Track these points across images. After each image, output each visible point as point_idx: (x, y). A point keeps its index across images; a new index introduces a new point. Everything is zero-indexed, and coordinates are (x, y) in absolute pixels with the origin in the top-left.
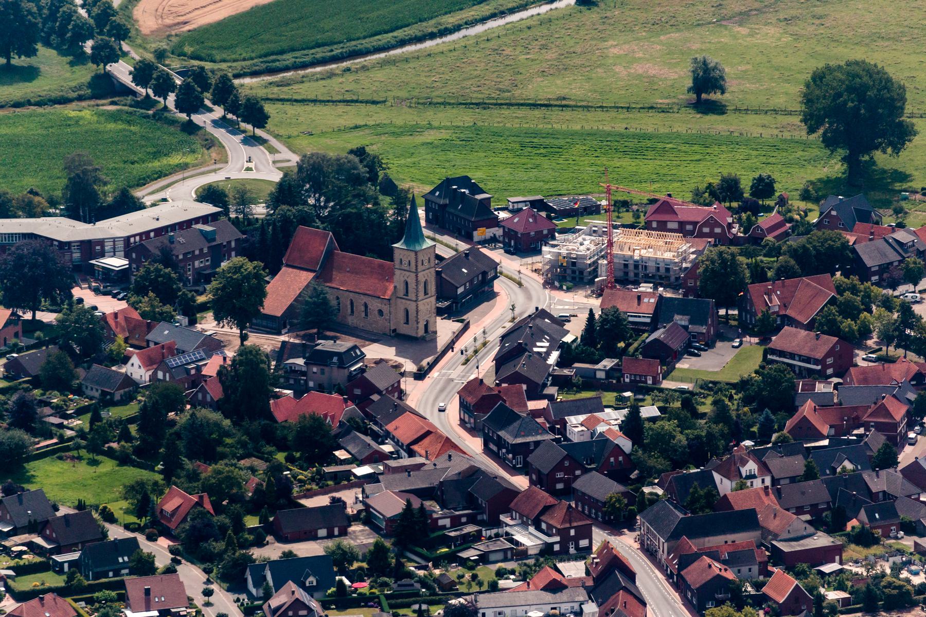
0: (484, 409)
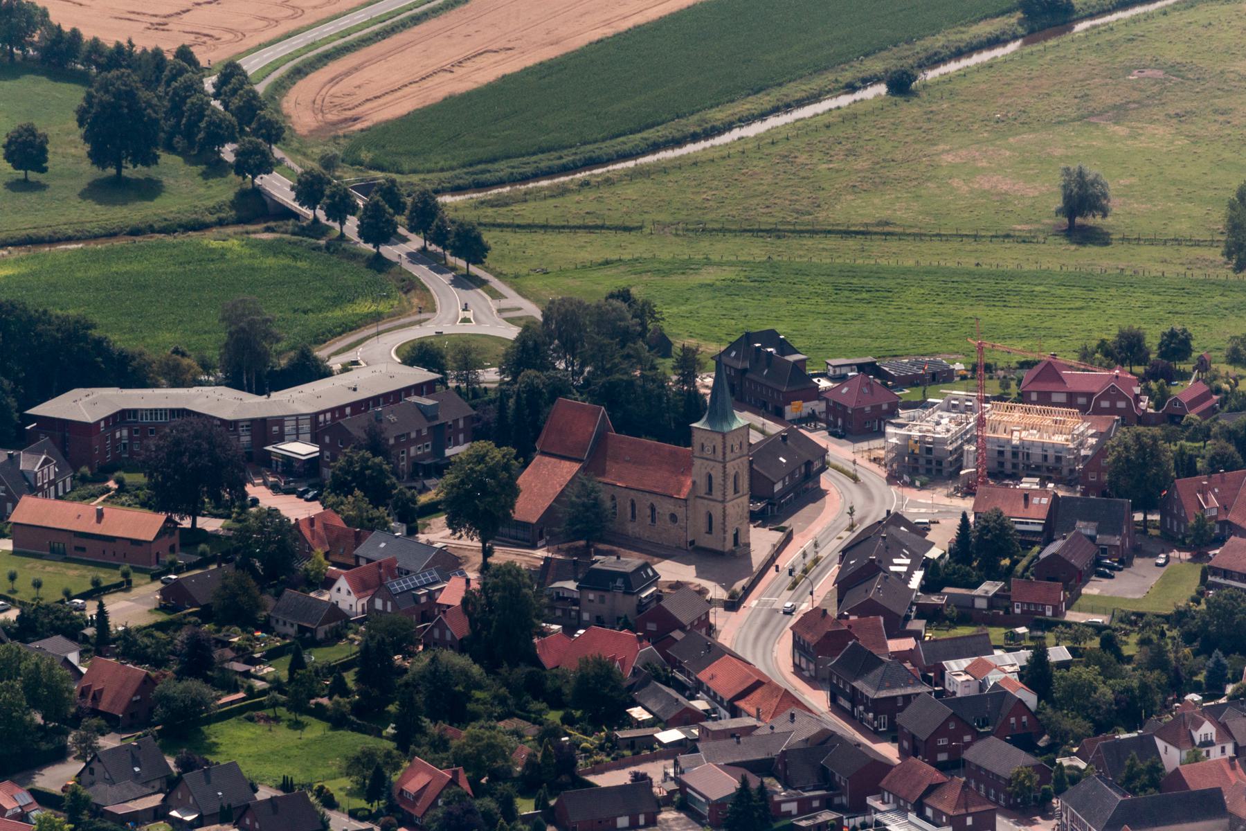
0: (829, 650)
